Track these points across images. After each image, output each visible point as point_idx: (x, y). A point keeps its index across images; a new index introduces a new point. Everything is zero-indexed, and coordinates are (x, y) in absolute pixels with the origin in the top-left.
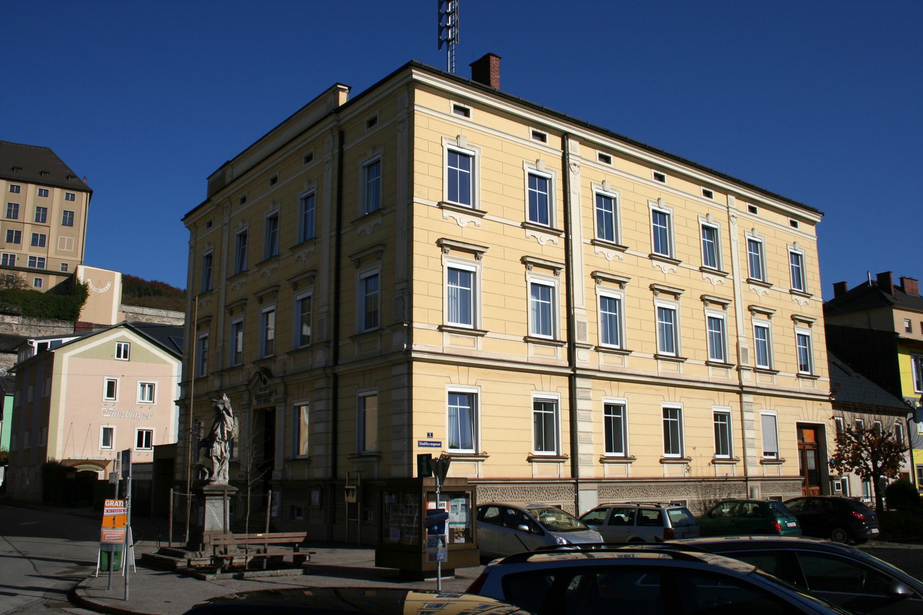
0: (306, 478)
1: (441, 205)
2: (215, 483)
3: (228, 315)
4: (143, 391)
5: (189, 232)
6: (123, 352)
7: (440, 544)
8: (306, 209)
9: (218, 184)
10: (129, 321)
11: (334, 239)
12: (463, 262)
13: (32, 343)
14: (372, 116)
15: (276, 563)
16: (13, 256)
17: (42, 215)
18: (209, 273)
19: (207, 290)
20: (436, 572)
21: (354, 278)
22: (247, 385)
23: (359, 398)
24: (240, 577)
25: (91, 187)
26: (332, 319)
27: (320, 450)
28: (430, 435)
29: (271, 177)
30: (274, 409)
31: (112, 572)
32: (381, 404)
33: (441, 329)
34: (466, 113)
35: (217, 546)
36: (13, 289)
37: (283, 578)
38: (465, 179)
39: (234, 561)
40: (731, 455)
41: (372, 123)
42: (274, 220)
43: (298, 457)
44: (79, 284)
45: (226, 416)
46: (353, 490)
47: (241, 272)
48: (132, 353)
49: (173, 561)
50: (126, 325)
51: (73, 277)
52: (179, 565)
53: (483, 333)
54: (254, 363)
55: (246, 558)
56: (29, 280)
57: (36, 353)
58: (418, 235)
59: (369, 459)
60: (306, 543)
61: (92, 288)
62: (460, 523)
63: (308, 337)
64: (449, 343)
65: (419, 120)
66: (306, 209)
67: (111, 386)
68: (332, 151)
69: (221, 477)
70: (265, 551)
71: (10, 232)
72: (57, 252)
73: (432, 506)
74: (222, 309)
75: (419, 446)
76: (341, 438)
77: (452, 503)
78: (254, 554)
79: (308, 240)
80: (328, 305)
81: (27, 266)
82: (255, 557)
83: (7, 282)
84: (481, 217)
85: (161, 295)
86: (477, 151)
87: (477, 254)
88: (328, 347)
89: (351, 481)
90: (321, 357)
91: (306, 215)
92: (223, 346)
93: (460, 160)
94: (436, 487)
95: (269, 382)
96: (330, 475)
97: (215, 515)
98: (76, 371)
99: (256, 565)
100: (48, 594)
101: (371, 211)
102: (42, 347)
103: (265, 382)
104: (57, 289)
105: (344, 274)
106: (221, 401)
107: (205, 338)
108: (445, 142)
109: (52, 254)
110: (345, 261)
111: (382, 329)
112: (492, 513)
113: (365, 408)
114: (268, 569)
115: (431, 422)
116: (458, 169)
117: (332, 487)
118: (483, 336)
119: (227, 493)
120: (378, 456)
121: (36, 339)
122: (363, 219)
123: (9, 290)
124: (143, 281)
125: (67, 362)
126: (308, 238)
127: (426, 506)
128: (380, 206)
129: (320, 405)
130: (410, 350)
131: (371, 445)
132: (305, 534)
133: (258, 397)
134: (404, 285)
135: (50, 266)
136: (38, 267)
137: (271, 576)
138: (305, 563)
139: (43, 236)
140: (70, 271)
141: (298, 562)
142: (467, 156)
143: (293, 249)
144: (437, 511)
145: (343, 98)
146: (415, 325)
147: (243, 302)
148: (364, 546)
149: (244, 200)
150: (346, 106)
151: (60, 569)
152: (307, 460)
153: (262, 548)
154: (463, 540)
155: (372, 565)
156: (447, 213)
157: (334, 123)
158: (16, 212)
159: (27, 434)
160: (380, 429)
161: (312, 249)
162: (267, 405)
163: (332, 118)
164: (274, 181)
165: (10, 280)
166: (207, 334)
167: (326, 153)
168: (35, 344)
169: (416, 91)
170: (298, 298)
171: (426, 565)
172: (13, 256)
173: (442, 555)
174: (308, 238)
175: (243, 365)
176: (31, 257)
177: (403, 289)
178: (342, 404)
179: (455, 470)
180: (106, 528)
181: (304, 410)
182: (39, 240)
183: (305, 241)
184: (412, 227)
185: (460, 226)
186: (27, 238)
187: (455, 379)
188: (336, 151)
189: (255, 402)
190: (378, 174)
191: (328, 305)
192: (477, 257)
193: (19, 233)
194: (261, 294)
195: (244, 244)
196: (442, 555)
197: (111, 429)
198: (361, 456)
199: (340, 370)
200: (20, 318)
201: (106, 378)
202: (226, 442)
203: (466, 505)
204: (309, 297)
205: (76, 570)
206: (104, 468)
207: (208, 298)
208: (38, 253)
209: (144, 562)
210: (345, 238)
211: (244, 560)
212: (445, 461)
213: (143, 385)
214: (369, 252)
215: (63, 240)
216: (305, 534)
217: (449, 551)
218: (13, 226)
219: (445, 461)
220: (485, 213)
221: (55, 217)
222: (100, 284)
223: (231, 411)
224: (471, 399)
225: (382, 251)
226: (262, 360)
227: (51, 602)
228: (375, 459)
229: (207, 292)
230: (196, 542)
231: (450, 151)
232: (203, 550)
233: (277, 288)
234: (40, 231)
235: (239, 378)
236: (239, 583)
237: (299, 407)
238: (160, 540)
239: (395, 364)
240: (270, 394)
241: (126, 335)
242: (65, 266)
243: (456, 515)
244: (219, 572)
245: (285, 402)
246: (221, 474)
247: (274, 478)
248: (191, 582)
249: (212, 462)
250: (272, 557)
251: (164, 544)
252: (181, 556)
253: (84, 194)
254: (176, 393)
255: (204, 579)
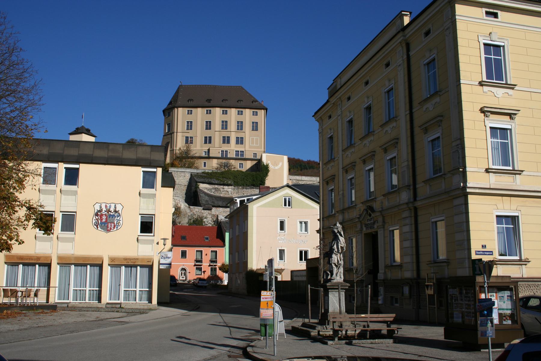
0: (400, 278)
1: (481, 84)
2: (334, 281)
3: (345, 173)
4: (301, 226)
5: (318, 123)
6: (288, 203)
7: (489, 324)
8: (389, 99)
9: (333, 91)
10: (290, 184)
11: (408, 116)
12: (502, 122)
13: (236, 200)
14: (427, 29)
15: (376, 335)
16: (226, 151)
17: (240, 125)
18: (332, 148)
19: (331, 159)
20: (488, 345)
21: (424, 141)
22: (359, 218)
23: (433, 222)
24: (350, 344)
25: (266, 106)
26: (411, 170)
27: (408, 259)
28: (484, 246)
29: (364, 81)
30: (377, 232)
31: (268, 337)
32: (447, 226)
33: (487, 171)
34: (495, 15)
35: (335, 322)
36: (228, 171)
37: (379, 345)
38: (498, 63)
39: (348, 332)
40: (520, 256)
41: (427, 33)
42: (369, 109)
43: (394, 264)
44: (264, 165)
45: (339, 236)
46: (431, 285)
47: (351, 145)
48: (293, 203)
49: (309, 331)
50: (288, 186)
51: (260, 161)
52: (312, 334)
53: (520, 172)
54: (362, 203)
55: (355, 331)
56: (236, 165)
57: (239, 206)
58: (466, 106)
59: (442, 264)
60: (396, 321)
61: (271, 167)
62: (507, 309)
63: (396, 186)
64: (494, 181)
65: (460, 26)
66: (389, 99)
67: (282, 224)
68: (402, 57)
69: (338, 277)
70: (368, 326)
71: (224, 137)
72: (250, 147)
73: (483, 296)
74: (341, 170)
75: (476, 254)
76: (422, 251)
77: (500, 294)
78: (362, 328)
79: (391, 119)
80: (408, 161)
81: (235, 157)
82: (362, 330)
83: (224, 167)
84: (513, 89)
85: (314, 169)
86: (506, 42)
87: (511, 116)
88: (409, 189)
89: (430, 279)
90: (405, 196)
91: (389, 103)
92: (343, 194)
93: (493, 51)
94: (484, 282)
95: (373, 215)
96: (415, 276)
97: (336, 302)
98: (262, 214)
99: (362, 336)
100: (232, 349)
101: (432, 93)
102: (242, 202)
103: (370, 215)
104: (252, 169)
105: (417, 139)
106: (336, 227)
107: (332, 190)
108: (481, 39)
109: (247, 148)
110: (417, 130)
111: (444, 174)
112: (534, 303)
113: (436, 229)
114: (370, 338)
115: (483, 236)
116: (492, 57)
117: (417, 284)
118: (520, 174)
119: (340, 287)
120: (447, 262)
121: (239, 198)
122: (426, 100)
123: (225, 171)
124: (302, 161)
125: (256, 210)
126: (392, 117)
127: (478, 296)
128: (438, 90)
129: (406, 229)
130: (465, 187)
131: (442, 256)
132: (394, 315)
133: (366, 225)
134: (458, 142)
135: (247, 156)
136: (240, 157)
137: (372, 343)
138: (394, 335)
139: (242, 138)
140: (258, 157)
141: (390, 335)
142: (499, 46)
143: (382, 126)
144: (486, 300)
145: (407, 20)
146: (468, 169)
147: (353, 164)
148: (439, 324)
149: (349, 99)
150: (409, 25)
151: (244, 334)
152: (400, 266)
153: (365, 324)
154: (509, 322)
155: (442, 338)
156: (486, 89)
157: (402, 38)
158: (226, 125)
159: (237, 254)
160: (448, 243)
161: (394, 124)
162: (373, 230)
163: (401, 34)
164: (367, 83)
165: (226, 165)
166: (333, 187)
167: (399, 59)
168: (238, 201)
169: (456, 5)
170: (388, 158)
171: (481, 341)
172: (226, 151)
173: (491, 332)
174: (392, 117)
175: (356, 205)
176: (236, 151)
177: (458, 145)
178: (421, 227)
179: (498, 271)
180: (262, 309)
181: (397, 233)
182: (240, 141)
183: (390, 119)
184: (461, 101)
185: (497, 97)
186: (233, 140)
187: (500, 206)
188: (405, 57)
189: (364, 229)
190: (434, 68)
191: (408, 161)
192: (511, 118)
193: (228, 137)
194: (364, 158)
195: (352, 127)
196: (491, 332)
197: (284, 250)
198: (436, 262)
199: (418, 204)
200: (233, 187)
201: (279, 219)
202: (340, 254)
203: (511, 297)
204: (395, 157)
205: (253, 335)
206: (281, 274)
207: (332, 164)
208: (240, 148)
209: (293, 331)
210: (415, 115)
211: (354, 332)
212: (490, 265)
213: (301, 223)
214: (432, 122)
215: (253, 139)
216: (394, 315)
217: (496, 330)
218: (226, 134)
219: (490, 265)
220: (515, 85)
221: (247, 126)
222: (276, 164)
223: (342, 233)
224: (514, 220)
225: (441, 121)
226: (368, 201)
227: (233, 354)
228: (445, 264)
229: (332, 160)
230: (324, 320)
231: (485, 45)
232: (328, 324)
233: (374, 153)
234: (240, 135)
235: (354, 214)
236: (349, 347)
237: (393, 231)
238: (304, 318)
239: (456, 198)
240: (374, 223)
241: (289, 192)
242: (255, 154)
243: (501, 304)
244: (336, 339)
245: (384, 228)
246: (338, 275)
247: (379, 278)
248: (319, 345)
249: (332, 267)
250: (371, 330)
251: (307, 320)
252: (314, 328)
253: (263, 111)
254: (317, 226)
255: (326, 343)
